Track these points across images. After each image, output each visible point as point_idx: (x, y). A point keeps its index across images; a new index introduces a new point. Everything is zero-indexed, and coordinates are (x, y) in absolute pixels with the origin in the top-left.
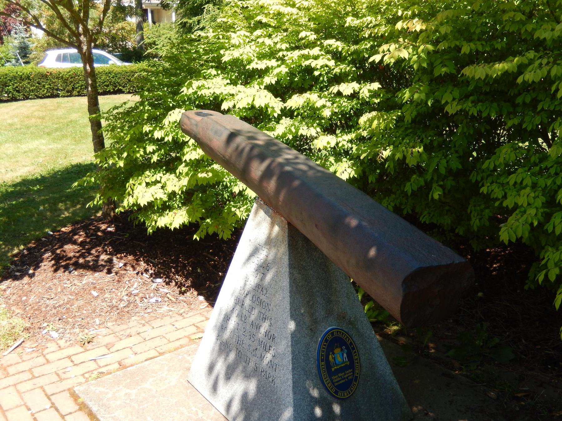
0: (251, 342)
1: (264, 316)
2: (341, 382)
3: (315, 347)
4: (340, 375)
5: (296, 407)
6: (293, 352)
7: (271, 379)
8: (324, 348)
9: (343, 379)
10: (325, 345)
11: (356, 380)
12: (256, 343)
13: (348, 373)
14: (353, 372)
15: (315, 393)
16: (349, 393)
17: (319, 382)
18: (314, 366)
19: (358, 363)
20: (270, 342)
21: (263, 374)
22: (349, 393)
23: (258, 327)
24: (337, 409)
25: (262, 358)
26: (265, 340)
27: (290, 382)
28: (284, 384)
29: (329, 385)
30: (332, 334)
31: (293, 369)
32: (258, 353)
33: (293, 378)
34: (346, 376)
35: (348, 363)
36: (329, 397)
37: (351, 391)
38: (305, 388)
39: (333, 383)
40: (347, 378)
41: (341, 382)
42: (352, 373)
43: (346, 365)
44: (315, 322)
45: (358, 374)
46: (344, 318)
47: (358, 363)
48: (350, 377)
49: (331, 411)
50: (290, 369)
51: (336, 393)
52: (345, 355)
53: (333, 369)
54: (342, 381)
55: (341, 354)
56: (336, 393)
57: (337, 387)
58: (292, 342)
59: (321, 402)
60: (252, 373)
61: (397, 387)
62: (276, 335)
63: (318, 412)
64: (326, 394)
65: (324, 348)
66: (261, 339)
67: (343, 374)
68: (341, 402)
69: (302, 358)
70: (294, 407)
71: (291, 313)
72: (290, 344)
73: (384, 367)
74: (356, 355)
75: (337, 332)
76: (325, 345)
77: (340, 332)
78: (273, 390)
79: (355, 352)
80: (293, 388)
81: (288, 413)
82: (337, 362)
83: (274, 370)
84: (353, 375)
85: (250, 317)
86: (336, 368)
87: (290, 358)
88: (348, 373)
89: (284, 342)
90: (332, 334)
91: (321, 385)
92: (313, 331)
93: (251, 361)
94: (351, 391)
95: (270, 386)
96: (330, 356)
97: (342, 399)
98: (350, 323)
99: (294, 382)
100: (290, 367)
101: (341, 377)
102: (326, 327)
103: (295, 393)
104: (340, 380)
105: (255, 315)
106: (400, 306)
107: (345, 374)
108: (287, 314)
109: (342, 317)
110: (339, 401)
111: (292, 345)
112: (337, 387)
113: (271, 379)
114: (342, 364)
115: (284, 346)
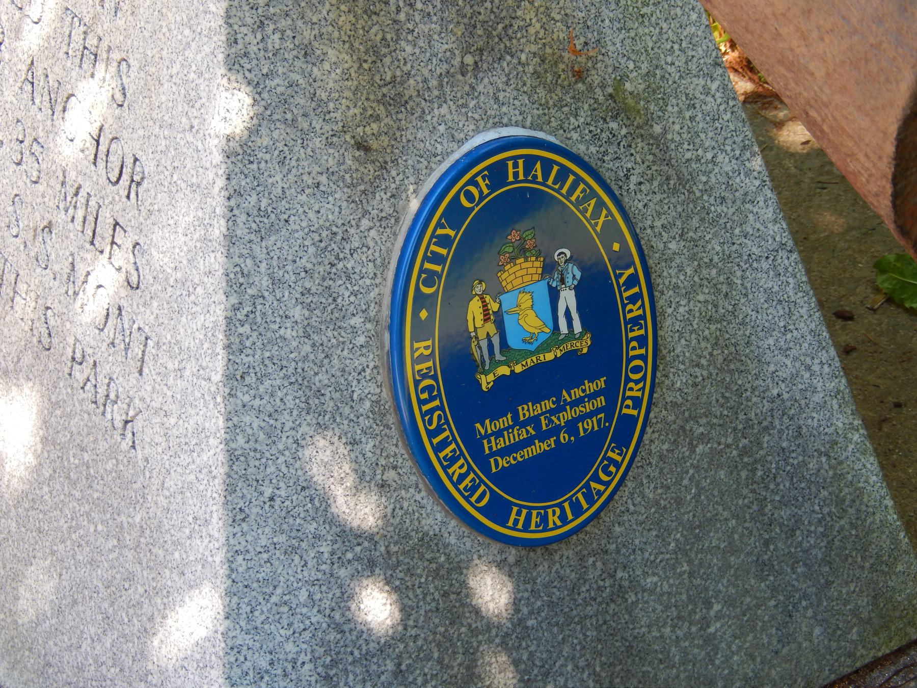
0: (22, 184)
1: (92, 41)
2: (528, 453)
3: (379, 249)
4: (526, 411)
5: (245, 596)
6: (237, 281)
7: (116, 413)
8: (437, 259)
9: (542, 436)
10: (444, 241)
11: (622, 441)
12: (48, 190)
13: (579, 402)
14: (611, 393)
15: (362, 511)
16: (577, 510)
17: (398, 449)
18: (371, 360)
19: (642, 341)
20: (114, 201)
21: (80, 374)
22: (577, 510)
23: (59, 102)
24: (492, 592)
25: (73, 280)
26: (94, 181)
27: (213, 454)
28: (185, 459)
29: (456, 469)
30: (497, 174)
31: (235, 377)
32: (59, 249)
33: (233, 429)
34: (569, 414)
35: (584, 345)
36: (454, 532)
37: (591, 501)
38: (305, 486)
39: (482, 461)
40: (571, 426)
41: (528, 453)
42: (601, 401)
43: (571, 355)
44: (394, 99)
45: (637, 403)
46: (580, 75)
47: (642, 341)
48: (591, 425)
49: (456, 603)
50: (217, 377)
51: (498, 510)
52: (568, 299)
53: (486, 381)
54: (540, 447)
55: (542, 289)
56: (498, 510)
57: (500, 478)
58: (231, 219)
59: (392, 556)
60: (27, 359)
61: (868, 470)
62: (148, 165)
63: (377, 607)
64: (434, 517)
65: (437, 259)
66: (72, 175)
67: (549, 404)
68: (524, 557)
69: (297, 313)
70: (229, 593)
71: (232, 41)
72: (219, 229)
73: (797, 358)
74: (633, 299)
75: (530, 162)
76: (444, 241)
77: (547, 165)
78: (128, 473)
79: (633, 281)
80: (230, 489)
81: (194, 621)
82: (514, 342)
83: (134, 365)
84: (609, 409)
85: (18, 32)
86: (504, 370)
87: (219, 313)
88: (579, 402)
89: (186, 213)
90: (497, 174)
91: (408, 465)
92: (372, 156)
93: (22, 287)
94: (591, 501)
95: (113, 451)
96: (475, 307)
97: (531, 545)
98: (619, 106)
99: (233, 457)
100: (217, 368)
101: (534, 421)
102: (456, 135)
103: (237, 516)
104: (528, 442)
105: (45, 29)
106: (893, 129)
107: (560, 409)
108: (211, 46)
109: (567, 72)
110: (512, 554)
111: (231, 239)
112: (500, 478)
113: (116, 413)
114: (545, 347)
115: (186, 232)
